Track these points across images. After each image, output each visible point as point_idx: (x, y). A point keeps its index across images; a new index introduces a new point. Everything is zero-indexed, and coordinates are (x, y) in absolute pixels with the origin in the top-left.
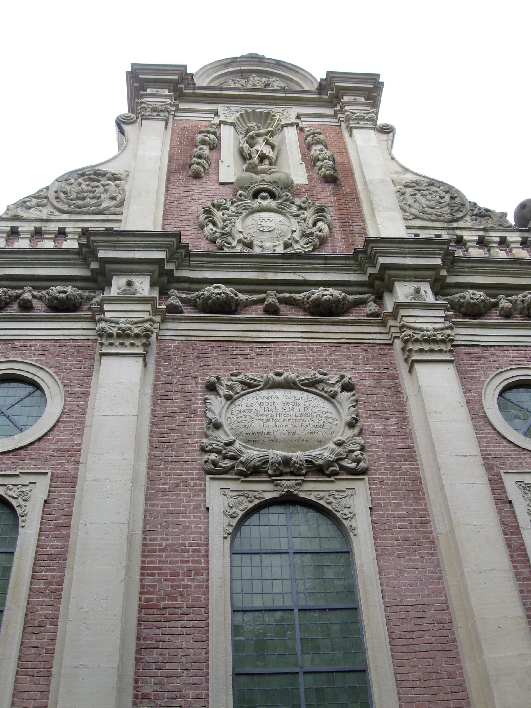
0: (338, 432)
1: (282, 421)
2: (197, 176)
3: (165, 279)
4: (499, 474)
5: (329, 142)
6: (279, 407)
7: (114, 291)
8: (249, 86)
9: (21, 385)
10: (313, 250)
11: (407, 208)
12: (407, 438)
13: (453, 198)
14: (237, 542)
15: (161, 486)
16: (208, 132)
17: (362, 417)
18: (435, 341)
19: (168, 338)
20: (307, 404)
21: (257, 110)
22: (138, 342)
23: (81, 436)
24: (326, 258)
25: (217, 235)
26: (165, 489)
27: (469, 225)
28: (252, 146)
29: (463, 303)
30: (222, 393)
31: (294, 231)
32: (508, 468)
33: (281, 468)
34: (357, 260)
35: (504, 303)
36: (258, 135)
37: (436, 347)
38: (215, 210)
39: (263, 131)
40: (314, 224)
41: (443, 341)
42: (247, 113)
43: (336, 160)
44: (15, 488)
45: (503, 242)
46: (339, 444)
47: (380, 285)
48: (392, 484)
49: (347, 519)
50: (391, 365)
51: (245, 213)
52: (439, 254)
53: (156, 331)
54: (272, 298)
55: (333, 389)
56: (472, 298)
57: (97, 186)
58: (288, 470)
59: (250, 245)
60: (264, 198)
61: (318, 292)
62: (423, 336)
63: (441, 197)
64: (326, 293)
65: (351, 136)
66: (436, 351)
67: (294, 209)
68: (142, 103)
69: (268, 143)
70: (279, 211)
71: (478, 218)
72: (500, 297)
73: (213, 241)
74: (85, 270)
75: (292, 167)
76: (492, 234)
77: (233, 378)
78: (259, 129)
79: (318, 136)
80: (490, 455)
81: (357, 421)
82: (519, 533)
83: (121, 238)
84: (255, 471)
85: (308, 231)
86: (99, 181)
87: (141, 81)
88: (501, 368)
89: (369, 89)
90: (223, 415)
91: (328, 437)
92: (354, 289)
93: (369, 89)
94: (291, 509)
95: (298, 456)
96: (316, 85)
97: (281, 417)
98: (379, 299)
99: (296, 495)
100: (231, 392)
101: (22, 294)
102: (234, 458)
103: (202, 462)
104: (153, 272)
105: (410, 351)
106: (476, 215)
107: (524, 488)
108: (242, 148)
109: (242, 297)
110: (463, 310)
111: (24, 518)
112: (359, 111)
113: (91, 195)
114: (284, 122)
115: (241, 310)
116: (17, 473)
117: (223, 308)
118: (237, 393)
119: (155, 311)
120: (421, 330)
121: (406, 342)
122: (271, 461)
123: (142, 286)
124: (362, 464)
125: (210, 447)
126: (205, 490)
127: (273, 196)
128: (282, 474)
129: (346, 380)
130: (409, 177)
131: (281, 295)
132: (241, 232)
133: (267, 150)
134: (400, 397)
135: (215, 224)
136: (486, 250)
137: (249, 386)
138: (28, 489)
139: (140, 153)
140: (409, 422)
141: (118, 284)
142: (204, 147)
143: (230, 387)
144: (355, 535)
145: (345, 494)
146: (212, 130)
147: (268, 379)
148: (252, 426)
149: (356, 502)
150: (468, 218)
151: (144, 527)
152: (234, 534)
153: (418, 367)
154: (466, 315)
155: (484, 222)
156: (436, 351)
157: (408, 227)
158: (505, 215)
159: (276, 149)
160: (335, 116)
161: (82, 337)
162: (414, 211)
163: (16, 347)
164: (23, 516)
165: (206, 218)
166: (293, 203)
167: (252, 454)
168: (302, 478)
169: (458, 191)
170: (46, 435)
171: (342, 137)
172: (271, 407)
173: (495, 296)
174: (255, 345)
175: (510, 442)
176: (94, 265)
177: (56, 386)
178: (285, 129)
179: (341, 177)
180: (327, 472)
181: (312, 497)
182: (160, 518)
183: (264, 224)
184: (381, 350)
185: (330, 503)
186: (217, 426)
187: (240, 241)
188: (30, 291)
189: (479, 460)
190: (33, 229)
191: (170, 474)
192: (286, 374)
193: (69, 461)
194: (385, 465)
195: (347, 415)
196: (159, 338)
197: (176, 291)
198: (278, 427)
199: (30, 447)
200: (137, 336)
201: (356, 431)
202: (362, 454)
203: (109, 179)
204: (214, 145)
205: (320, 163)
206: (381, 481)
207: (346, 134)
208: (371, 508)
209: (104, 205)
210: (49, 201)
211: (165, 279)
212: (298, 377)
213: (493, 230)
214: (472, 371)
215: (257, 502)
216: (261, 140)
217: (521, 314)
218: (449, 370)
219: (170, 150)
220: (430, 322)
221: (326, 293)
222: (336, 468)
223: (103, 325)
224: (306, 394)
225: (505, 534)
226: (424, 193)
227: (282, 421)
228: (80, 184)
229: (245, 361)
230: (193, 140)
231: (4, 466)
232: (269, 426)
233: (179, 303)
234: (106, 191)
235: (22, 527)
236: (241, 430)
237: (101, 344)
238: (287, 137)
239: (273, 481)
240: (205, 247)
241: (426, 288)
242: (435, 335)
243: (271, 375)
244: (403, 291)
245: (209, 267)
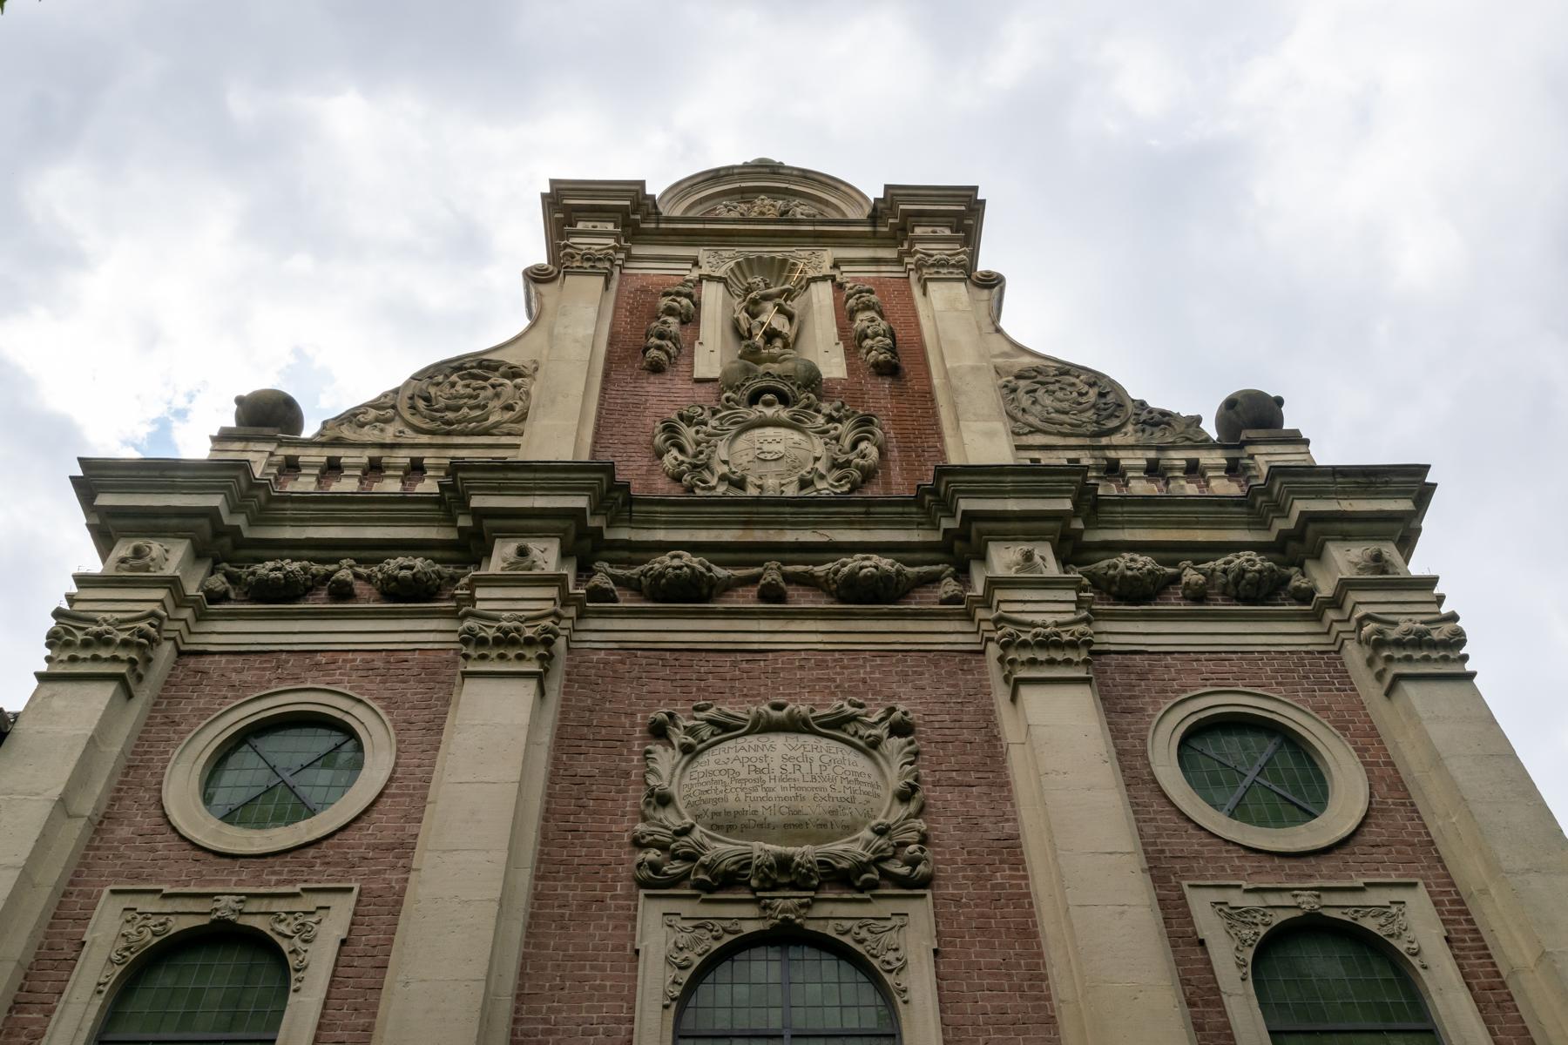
0: (880, 810)
1: (778, 789)
2: (656, 368)
3: (587, 544)
4: (1179, 887)
5: (887, 308)
6: (776, 765)
7: (495, 566)
8: (753, 215)
9: (306, 731)
10: (851, 491)
11: (1019, 415)
12: (1007, 820)
13: (1102, 395)
14: (689, 1016)
15: (556, 911)
16: (679, 294)
17: (926, 783)
18: (1059, 645)
19: (588, 645)
20: (826, 759)
21: (766, 256)
22: (529, 653)
23: (420, 821)
24: (868, 503)
25: (683, 467)
26: (562, 916)
27: (1131, 440)
28: (754, 316)
29: (1114, 577)
30: (676, 743)
31: (817, 459)
32: (1197, 878)
33: (774, 876)
34: (922, 506)
35: (1191, 576)
36: (766, 298)
37: (1059, 656)
38: (683, 426)
39: (773, 290)
40: (854, 446)
41: (1073, 645)
42: (747, 260)
43: (899, 335)
44: (290, 918)
45: (1193, 469)
46: (881, 831)
47: (963, 549)
48: (976, 906)
49: (890, 971)
50: (983, 691)
51: (735, 429)
52: (1069, 491)
53: (566, 632)
54: (772, 573)
55: (873, 732)
56: (1129, 568)
57: (484, 388)
58: (785, 880)
59: (740, 484)
60: (768, 404)
61: (853, 562)
62: (1036, 635)
63: (1081, 394)
64: (866, 563)
65: (925, 294)
66: (1059, 663)
67: (821, 420)
68: (566, 246)
69: (781, 310)
70: (795, 425)
71: (1147, 427)
72: (1183, 564)
73: (677, 478)
74: (448, 530)
75: (821, 349)
76: (1173, 454)
77: (697, 715)
78: (767, 286)
79: (866, 297)
80: (1163, 851)
81: (914, 789)
82: (1220, 1003)
83: (510, 475)
84: (726, 881)
85: (842, 458)
86: (486, 379)
87: (567, 207)
88: (1185, 692)
89: (961, 212)
90: (676, 780)
91: (861, 819)
92: (918, 556)
93: (961, 212)
94: (794, 953)
95: (803, 852)
96: (868, 210)
97: (777, 782)
98: (962, 574)
99: (800, 926)
100: (690, 740)
101: (336, 571)
102: (690, 857)
103: (634, 866)
104: (565, 531)
105: (1012, 662)
106: (1144, 422)
107: (1229, 916)
108: (737, 320)
109: (721, 572)
110: (1114, 589)
111: (300, 975)
112: (939, 251)
113: (472, 402)
114: (811, 274)
115: (720, 595)
116: (297, 889)
117: (687, 593)
118: (703, 741)
119: (566, 600)
120: (1033, 625)
121: (1005, 646)
122: (756, 862)
123: (545, 556)
124: (921, 868)
125: (649, 838)
126: (634, 918)
127: (784, 400)
128: (776, 887)
129: (897, 715)
130: (1027, 361)
131: (790, 568)
132: (725, 462)
133: (780, 323)
134: (995, 746)
135: (682, 450)
136: (1161, 483)
137: (726, 728)
138: (315, 919)
139: (558, 330)
140: (1010, 791)
141: (502, 554)
142: (670, 319)
143: (691, 731)
144: (906, 1002)
145: (889, 924)
146: (686, 290)
147: (759, 715)
148: (726, 800)
149: (911, 937)
150: (1130, 428)
151: (521, 987)
152: (683, 1000)
153: (1025, 692)
154: (1120, 598)
155: (1158, 434)
156: (1059, 663)
157: (1019, 448)
158: (1197, 420)
159: (796, 320)
160: (899, 261)
161: (437, 646)
162: (1031, 419)
163: (318, 664)
164: (297, 971)
165: (666, 440)
166: (818, 411)
167: (723, 849)
168: (812, 894)
169: (1113, 382)
170: (357, 819)
171: (911, 297)
172: (759, 765)
173: (1174, 564)
174: (739, 657)
175: (1201, 828)
176: (464, 521)
177: (383, 732)
178: (813, 286)
179: (905, 365)
180: (858, 884)
181: (830, 930)
182: (549, 971)
183: (766, 447)
184: (963, 662)
185: (861, 942)
186: (664, 800)
187: (723, 478)
188: (351, 567)
189: (1137, 862)
190: (365, 460)
191: (574, 888)
192: (791, 706)
193: (394, 867)
194: (965, 870)
195: (896, 777)
196: (573, 645)
197: (606, 565)
198: (771, 800)
199: (325, 844)
200: (530, 642)
201: (913, 807)
202: (922, 851)
203: (504, 376)
204: (687, 316)
205: (868, 343)
206: (957, 901)
207: (916, 291)
208: (936, 952)
209: (492, 419)
210: (398, 413)
211: (587, 544)
212: (812, 711)
213: (1173, 447)
214: (1130, 697)
215: (728, 938)
216: (769, 305)
217: (1224, 593)
218: (1083, 698)
219: (613, 325)
220: (1050, 611)
221: (866, 563)
222: (874, 875)
223: (468, 623)
224: (825, 742)
225: (1191, 1004)
226: (1051, 387)
227: (778, 789)
228: (453, 385)
229: (719, 683)
230: (653, 306)
231: (274, 878)
232: (755, 799)
233: (611, 585)
234: (497, 395)
235: (296, 991)
236: (706, 806)
237: (466, 657)
238: (815, 300)
239: (757, 901)
240: (663, 487)
241: (1044, 552)
242: (1057, 634)
243: (766, 707)
244: (1003, 559)
245: (666, 522)
